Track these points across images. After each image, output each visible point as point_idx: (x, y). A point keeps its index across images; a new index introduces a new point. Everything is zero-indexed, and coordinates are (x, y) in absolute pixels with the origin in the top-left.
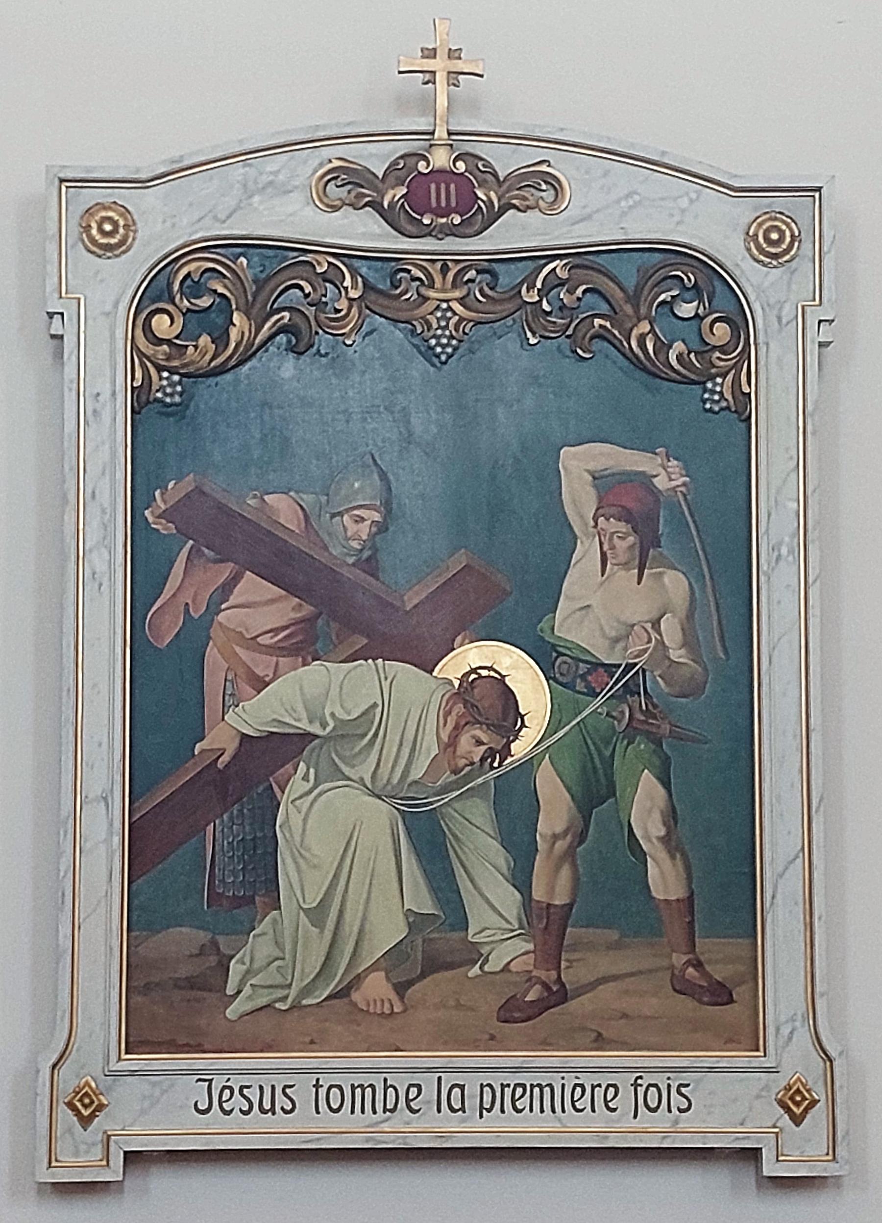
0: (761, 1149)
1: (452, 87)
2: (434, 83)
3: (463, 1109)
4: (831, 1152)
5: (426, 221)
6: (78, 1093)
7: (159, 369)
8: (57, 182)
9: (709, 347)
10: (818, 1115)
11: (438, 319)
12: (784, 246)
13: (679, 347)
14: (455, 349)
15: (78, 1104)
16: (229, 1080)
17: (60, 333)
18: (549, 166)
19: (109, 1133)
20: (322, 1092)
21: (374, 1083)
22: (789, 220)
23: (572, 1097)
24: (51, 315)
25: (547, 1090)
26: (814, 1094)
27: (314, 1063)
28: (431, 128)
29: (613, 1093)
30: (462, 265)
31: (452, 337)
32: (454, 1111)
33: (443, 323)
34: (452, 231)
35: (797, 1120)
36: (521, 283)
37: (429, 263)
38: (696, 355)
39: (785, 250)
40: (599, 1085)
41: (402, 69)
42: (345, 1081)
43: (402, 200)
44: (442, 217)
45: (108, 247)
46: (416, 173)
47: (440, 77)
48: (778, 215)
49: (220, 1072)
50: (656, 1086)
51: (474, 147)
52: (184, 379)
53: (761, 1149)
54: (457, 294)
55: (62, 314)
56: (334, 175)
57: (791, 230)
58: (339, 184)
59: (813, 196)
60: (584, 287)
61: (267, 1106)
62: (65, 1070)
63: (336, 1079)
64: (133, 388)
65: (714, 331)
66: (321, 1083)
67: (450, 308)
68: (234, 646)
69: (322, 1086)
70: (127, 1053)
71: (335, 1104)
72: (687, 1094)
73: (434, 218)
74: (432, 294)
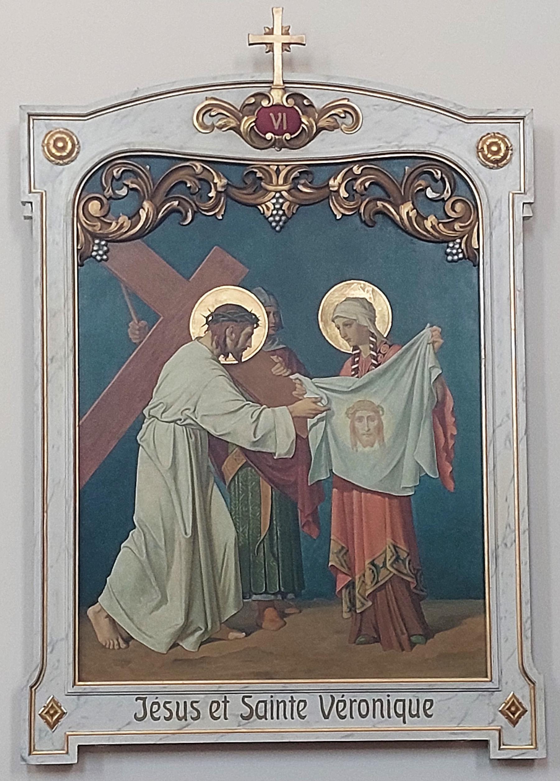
1: (285, 52)
5: (269, 139)
6: (506, 704)
8: (27, 116)
10: (525, 721)
11: (274, 204)
13: (432, 218)
17: (30, 215)
18: (348, 101)
19: (68, 733)
20: (295, 704)
24: (24, 203)
29: (303, 706)
30: (289, 168)
33: (278, 206)
34: (290, 145)
40: (355, 701)
42: (266, 697)
43: (253, 124)
45: (497, 162)
46: (261, 107)
49: (152, 693)
50: (365, 701)
52: (109, 244)
55: (31, 203)
56: (207, 110)
59: (519, 123)
60: (371, 181)
61: (181, 714)
64: (78, 249)
66: (228, 700)
67: (282, 196)
68: (377, 441)
70: (79, 681)
71: (400, 711)
73: (273, 136)
74: (270, 188)
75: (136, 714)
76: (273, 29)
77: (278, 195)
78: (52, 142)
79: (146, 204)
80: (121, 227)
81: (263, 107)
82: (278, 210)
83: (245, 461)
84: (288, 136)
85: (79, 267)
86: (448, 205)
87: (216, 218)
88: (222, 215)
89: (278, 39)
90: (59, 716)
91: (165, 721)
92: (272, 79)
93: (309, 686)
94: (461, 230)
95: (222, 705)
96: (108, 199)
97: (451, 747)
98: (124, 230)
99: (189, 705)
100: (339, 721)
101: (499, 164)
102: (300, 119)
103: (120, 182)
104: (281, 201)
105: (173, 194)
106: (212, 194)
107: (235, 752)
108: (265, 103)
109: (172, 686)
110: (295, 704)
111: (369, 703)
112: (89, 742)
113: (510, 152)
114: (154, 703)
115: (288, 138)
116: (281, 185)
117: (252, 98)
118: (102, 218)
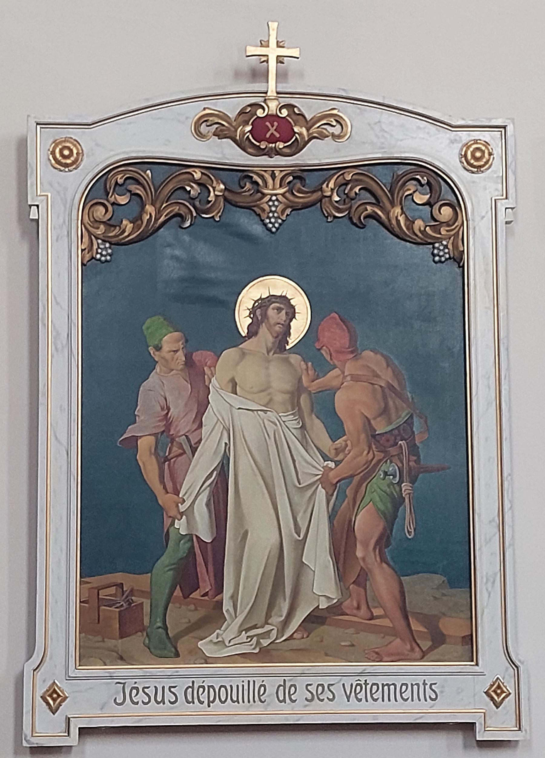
0: (475, 723)
4: (518, 726)
8: (35, 124)
14: (280, 224)
16: (204, 681)
17: (37, 218)
20: (369, 687)
21: (396, 683)
23: (289, 692)
24: (30, 206)
25: (392, 687)
26: (65, 693)
27: (423, 670)
28: (264, 90)
31: (279, 217)
32: (234, 702)
34: (278, 153)
36: (323, 183)
41: (248, 54)
42: (381, 680)
44: (272, 143)
46: (255, 117)
51: (296, 102)
52: (112, 246)
53: (475, 723)
54: (282, 191)
58: (208, 124)
59: (501, 131)
60: (360, 187)
61: (159, 699)
62: (39, 675)
66: (368, 682)
67: (277, 200)
69: (427, 684)
70: (79, 666)
74: (266, 191)
75: (116, 698)
77: (274, 198)
78: (57, 151)
79: (150, 208)
80: (124, 231)
81: (258, 117)
82: (274, 212)
83: (422, 462)
85: (83, 267)
86: (436, 209)
87: (215, 220)
89: (273, 52)
94: (448, 233)
95: (364, 686)
98: (126, 234)
99: (427, 687)
103: (123, 188)
104: (271, 203)
107: (377, 732)
108: (260, 113)
110: (369, 687)
114: (292, 686)
118: (108, 222)
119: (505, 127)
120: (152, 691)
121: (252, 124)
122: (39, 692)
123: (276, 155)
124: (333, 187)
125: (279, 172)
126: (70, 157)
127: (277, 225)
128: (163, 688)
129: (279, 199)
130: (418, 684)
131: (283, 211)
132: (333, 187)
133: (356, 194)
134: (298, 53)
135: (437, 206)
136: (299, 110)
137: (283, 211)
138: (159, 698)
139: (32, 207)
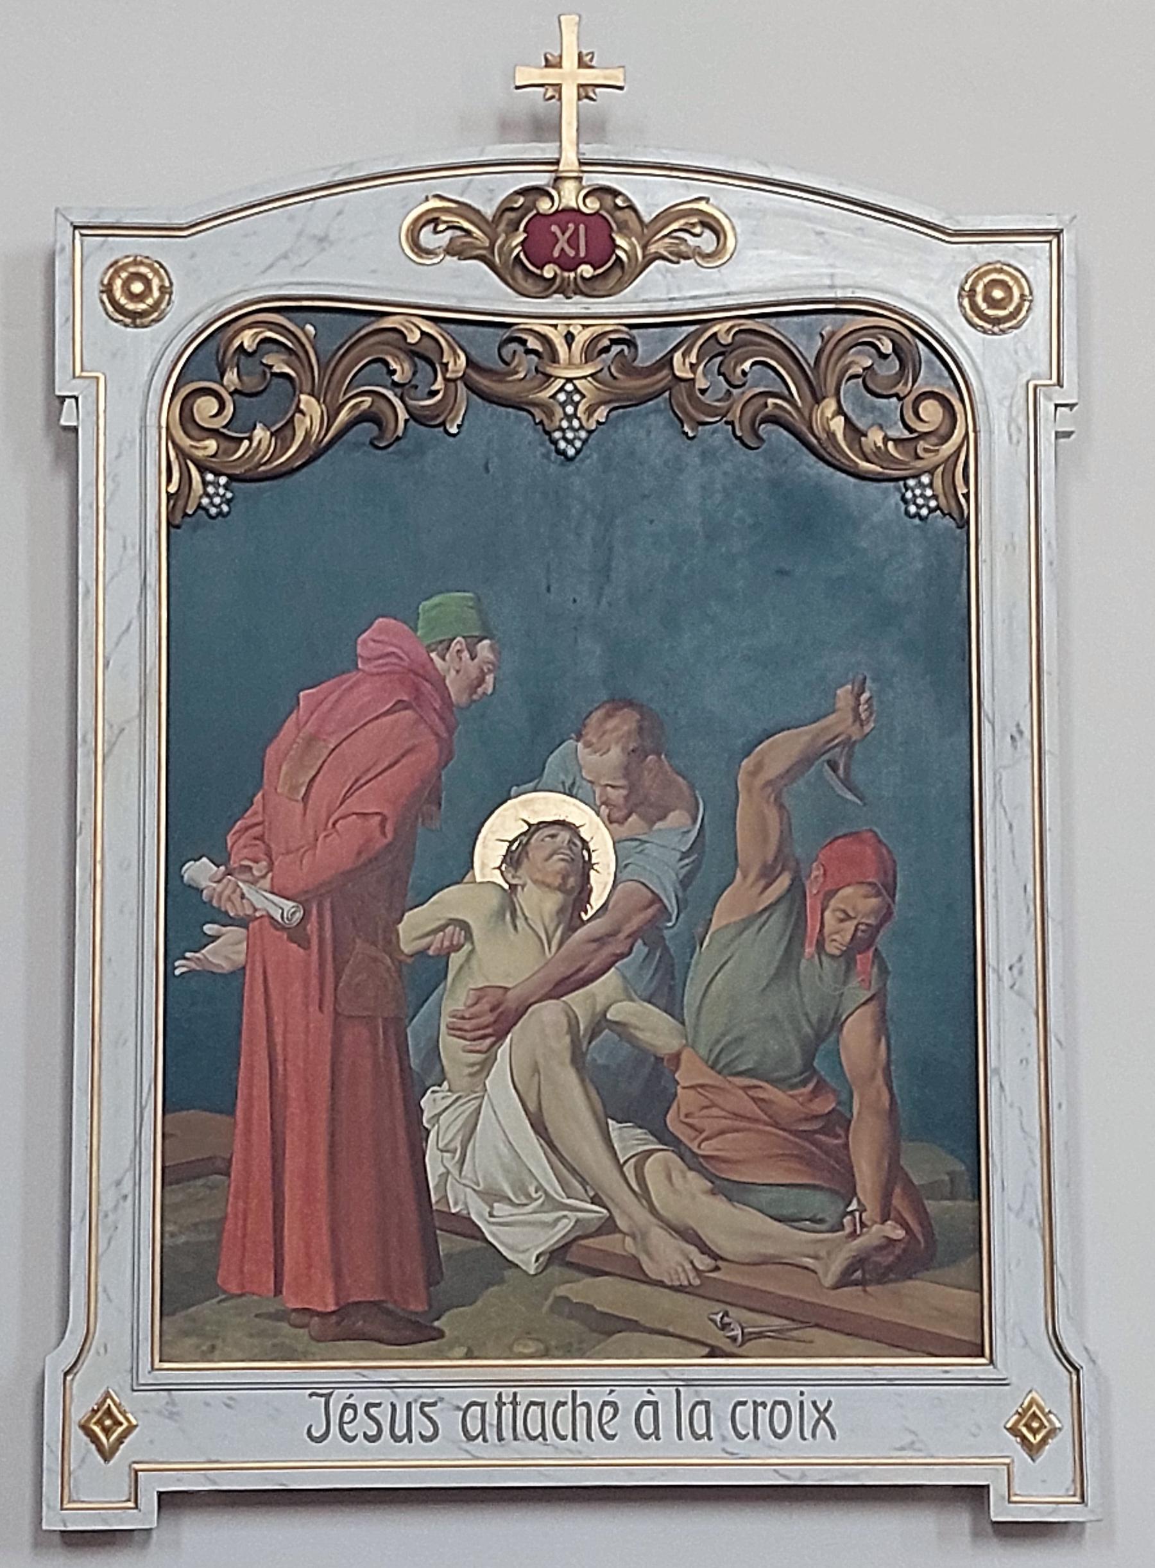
0: (988, 1486)
1: (586, 101)
2: (560, 99)
3: (708, 1434)
7: (202, 470)
9: (915, 435)
10: (1060, 1447)
12: (150, 301)
14: (585, 442)
15: (1024, 1430)
16: (351, 1395)
17: (75, 424)
22: (1019, 275)
24: (63, 399)
34: (585, 288)
35: (1032, 1450)
37: (552, 329)
38: (896, 446)
39: (1011, 313)
41: (518, 84)
42: (760, 1393)
44: (570, 270)
45: (135, 315)
46: (534, 212)
47: (569, 93)
48: (1005, 268)
50: (785, 1403)
51: (617, 180)
52: (234, 484)
53: (988, 1486)
55: (76, 398)
56: (432, 220)
57: (1021, 287)
61: (400, 1430)
62: (77, 1382)
63: (538, 1394)
65: (922, 416)
66: (518, 1400)
71: (648, 1429)
72: (376, 1415)
73: (559, 271)
75: (310, 1427)
76: (561, 57)
78: (118, 283)
81: (538, 214)
84: (586, 270)
85: (172, 530)
88: (459, 426)
89: (570, 76)
90: (124, 1431)
91: (366, 1442)
92: (557, 156)
93: (235, 1376)
96: (231, 394)
97: (921, 1499)
99: (415, 1409)
100: (424, 1447)
101: (138, 321)
102: (613, 240)
105: (358, 387)
106: (439, 385)
108: (544, 205)
109: (454, 1370)
111: (792, 1408)
112: (652, 1479)
113: (1027, 304)
115: (587, 275)
116: (578, 367)
117: (516, 197)
118: (225, 431)
119: (1058, 234)
120: (383, 1414)
121: (525, 231)
122: (78, 1414)
123: (575, 294)
124: (694, 361)
125: (580, 328)
126: (146, 297)
127: (578, 444)
128: (409, 1405)
129: (579, 387)
130: (708, 1403)
131: (590, 411)
132: (694, 361)
133: (744, 373)
134: (622, 77)
135: (909, 400)
136: (627, 199)
137: (590, 411)
138: (400, 1430)
139: (67, 400)
